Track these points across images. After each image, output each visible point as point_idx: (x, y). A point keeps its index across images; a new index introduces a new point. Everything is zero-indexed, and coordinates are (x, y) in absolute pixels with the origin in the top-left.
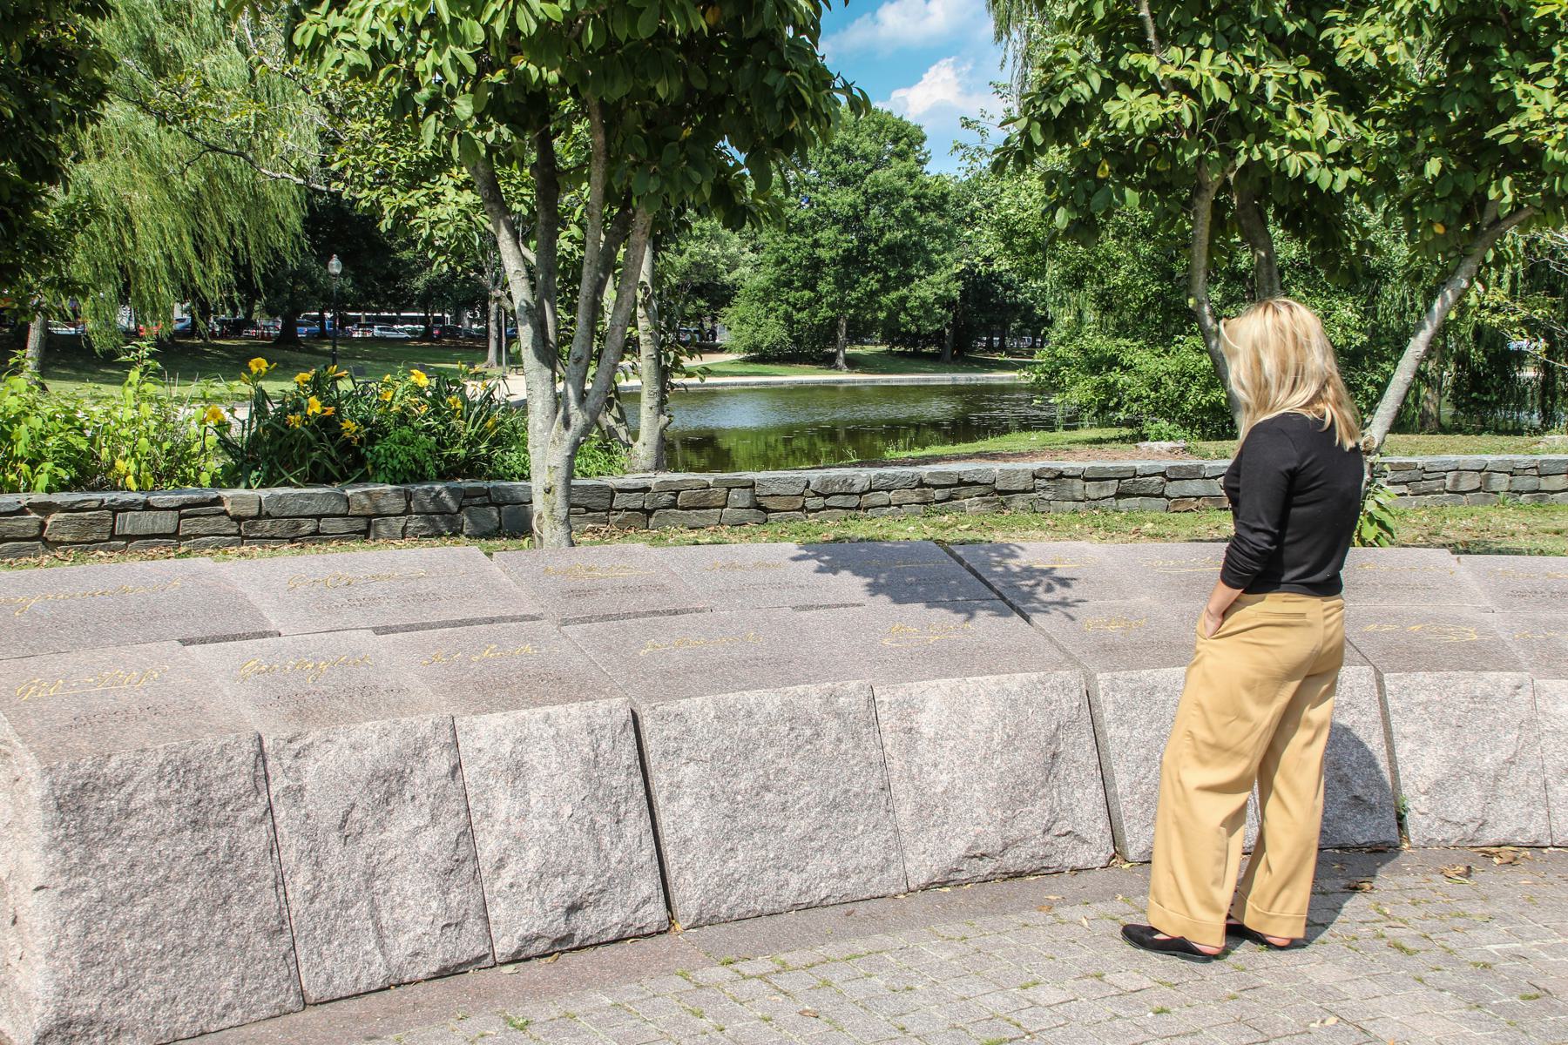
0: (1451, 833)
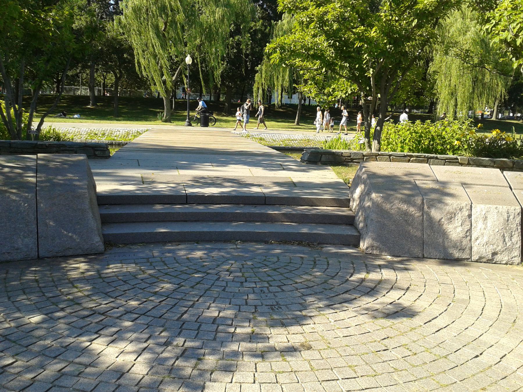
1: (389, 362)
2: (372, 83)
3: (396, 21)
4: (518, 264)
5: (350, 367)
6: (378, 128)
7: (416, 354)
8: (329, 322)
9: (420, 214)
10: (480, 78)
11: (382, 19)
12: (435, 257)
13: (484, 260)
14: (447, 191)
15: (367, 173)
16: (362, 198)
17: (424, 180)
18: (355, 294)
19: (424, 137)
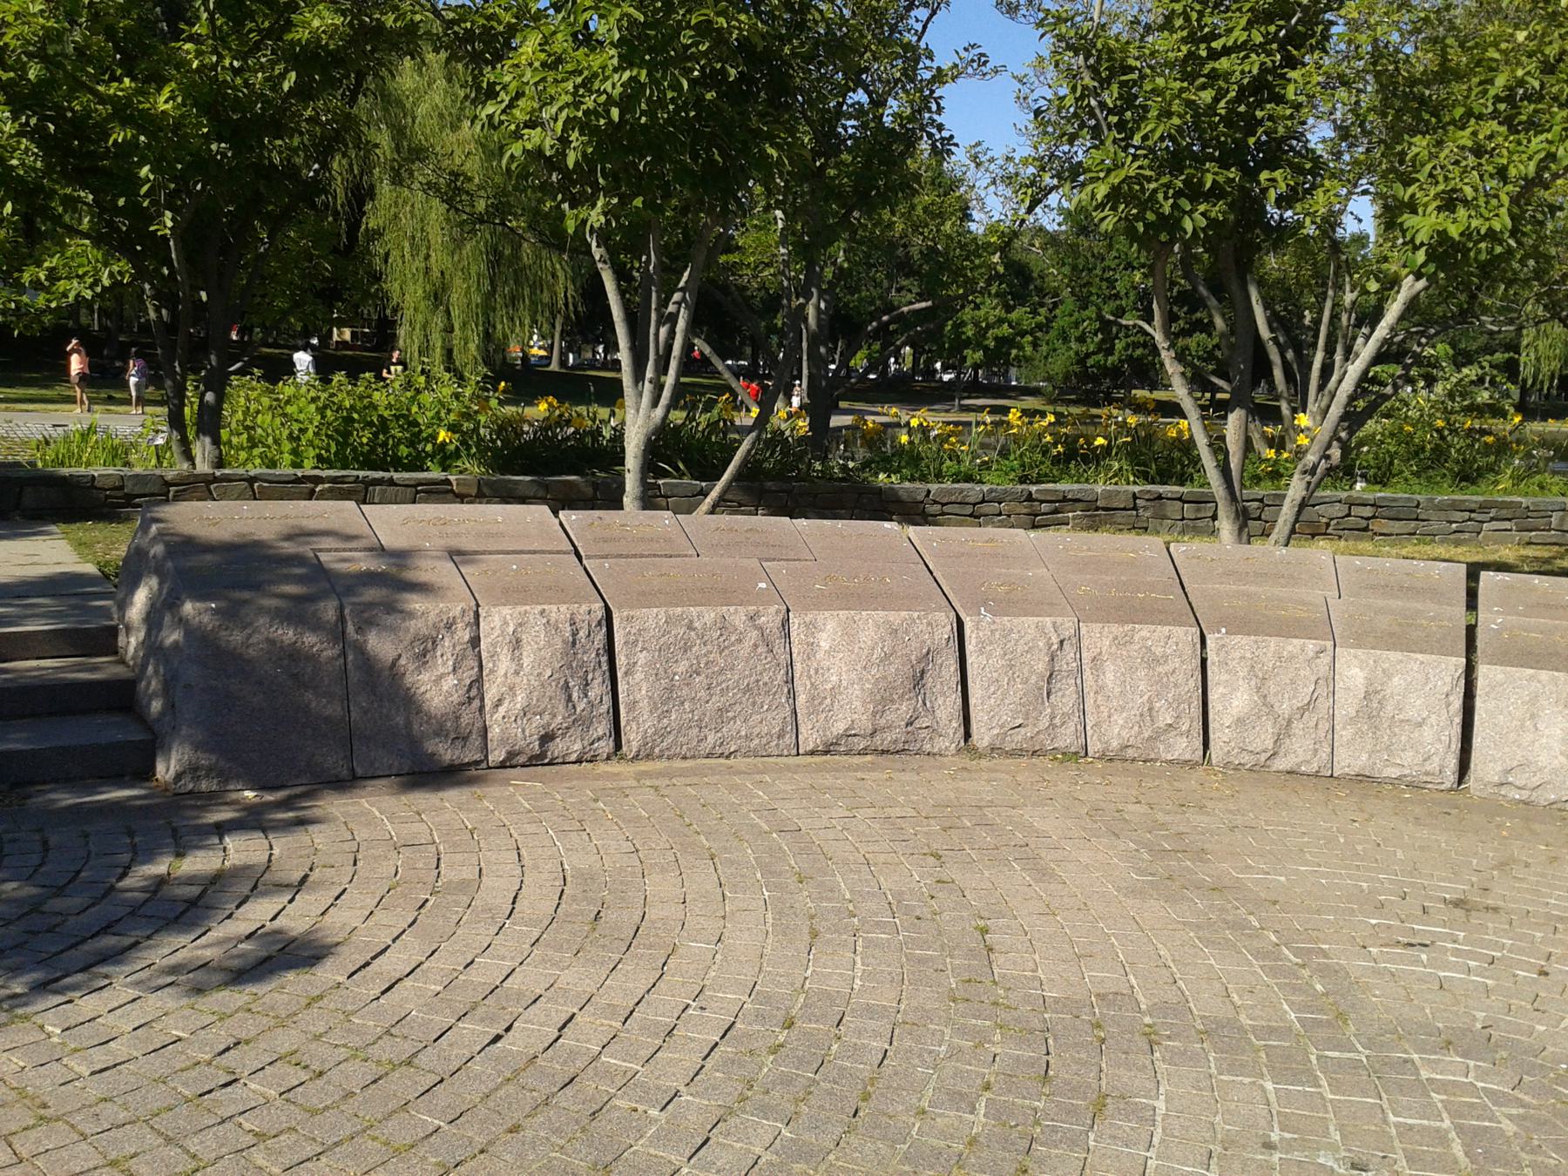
0: (1246, 759)
1: (241, 1119)
2: (173, 256)
3: (237, 72)
4: (608, 758)
5: (113, 1164)
6: (210, 397)
7: (321, 1074)
8: (44, 1036)
9: (336, 651)
10: (507, 252)
11: (190, 63)
12: (387, 773)
13: (522, 759)
14: (411, 575)
15: (167, 538)
16: (153, 619)
17: (344, 550)
18: (135, 929)
19: (359, 422)
